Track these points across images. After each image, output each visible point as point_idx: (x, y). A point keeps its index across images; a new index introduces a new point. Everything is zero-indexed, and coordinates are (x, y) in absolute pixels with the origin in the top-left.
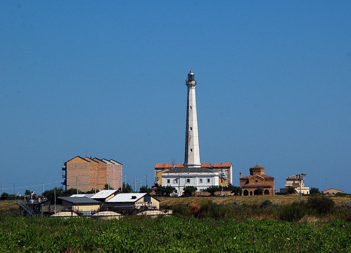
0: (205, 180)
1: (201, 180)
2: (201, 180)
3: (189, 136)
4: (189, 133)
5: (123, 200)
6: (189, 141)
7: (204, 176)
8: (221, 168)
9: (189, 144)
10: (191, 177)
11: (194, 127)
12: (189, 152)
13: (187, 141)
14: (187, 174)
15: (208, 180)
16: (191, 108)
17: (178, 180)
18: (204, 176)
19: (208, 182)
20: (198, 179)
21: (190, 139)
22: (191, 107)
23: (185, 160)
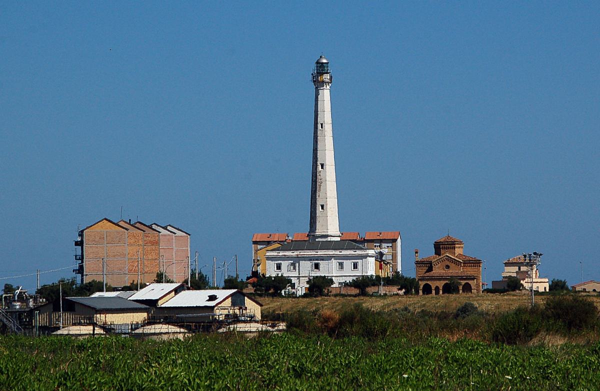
1: (341, 265)
2: (341, 265)
9: (319, 196)
10: (323, 260)
16: (322, 127)
17: (297, 264)
19: (354, 268)
20: (334, 263)
22: (322, 124)
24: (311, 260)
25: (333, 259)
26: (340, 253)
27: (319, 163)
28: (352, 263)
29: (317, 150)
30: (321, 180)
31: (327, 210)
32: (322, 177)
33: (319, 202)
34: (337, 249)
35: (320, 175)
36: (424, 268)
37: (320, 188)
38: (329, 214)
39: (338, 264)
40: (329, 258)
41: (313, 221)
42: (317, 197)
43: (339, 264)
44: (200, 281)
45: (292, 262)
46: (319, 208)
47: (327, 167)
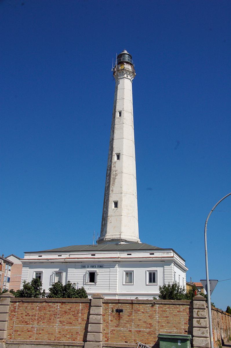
0: (141, 274)
1: (129, 274)
2: (129, 274)
3: (113, 173)
4: (113, 166)
5: (195, 331)
6: (111, 182)
7: (140, 263)
8: (200, 288)
9: (112, 191)
10: (101, 267)
11: (124, 171)
12: (110, 210)
13: (107, 185)
14: (90, 256)
15: (150, 274)
16: (120, 116)
17: (64, 274)
18: (140, 263)
19: (150, 281)
20: (119, 272)
21: (114, 179)
22: (120, 113)
23: (102, 232)
24: (84, 267)
25: (117, 266)
26: (40, 258)
27: (114, 153)
28: (148, 273)
29: (117, 89)
30: (116, 171)
31: (121, 207)
32: (116, 168)
33: (113, 198)
34: (110, 168)
35: (115, 167)
36: (173, 269)
37: (114, 181)
38: (125, 121)
39: (124, 273)
40: (111, 264)
41: (105, 224)
42: (111, 192)
43: (127, 274)
44: (29, 266)
45: (57, 270)
46: (112, 205)
47: (123, 157)
